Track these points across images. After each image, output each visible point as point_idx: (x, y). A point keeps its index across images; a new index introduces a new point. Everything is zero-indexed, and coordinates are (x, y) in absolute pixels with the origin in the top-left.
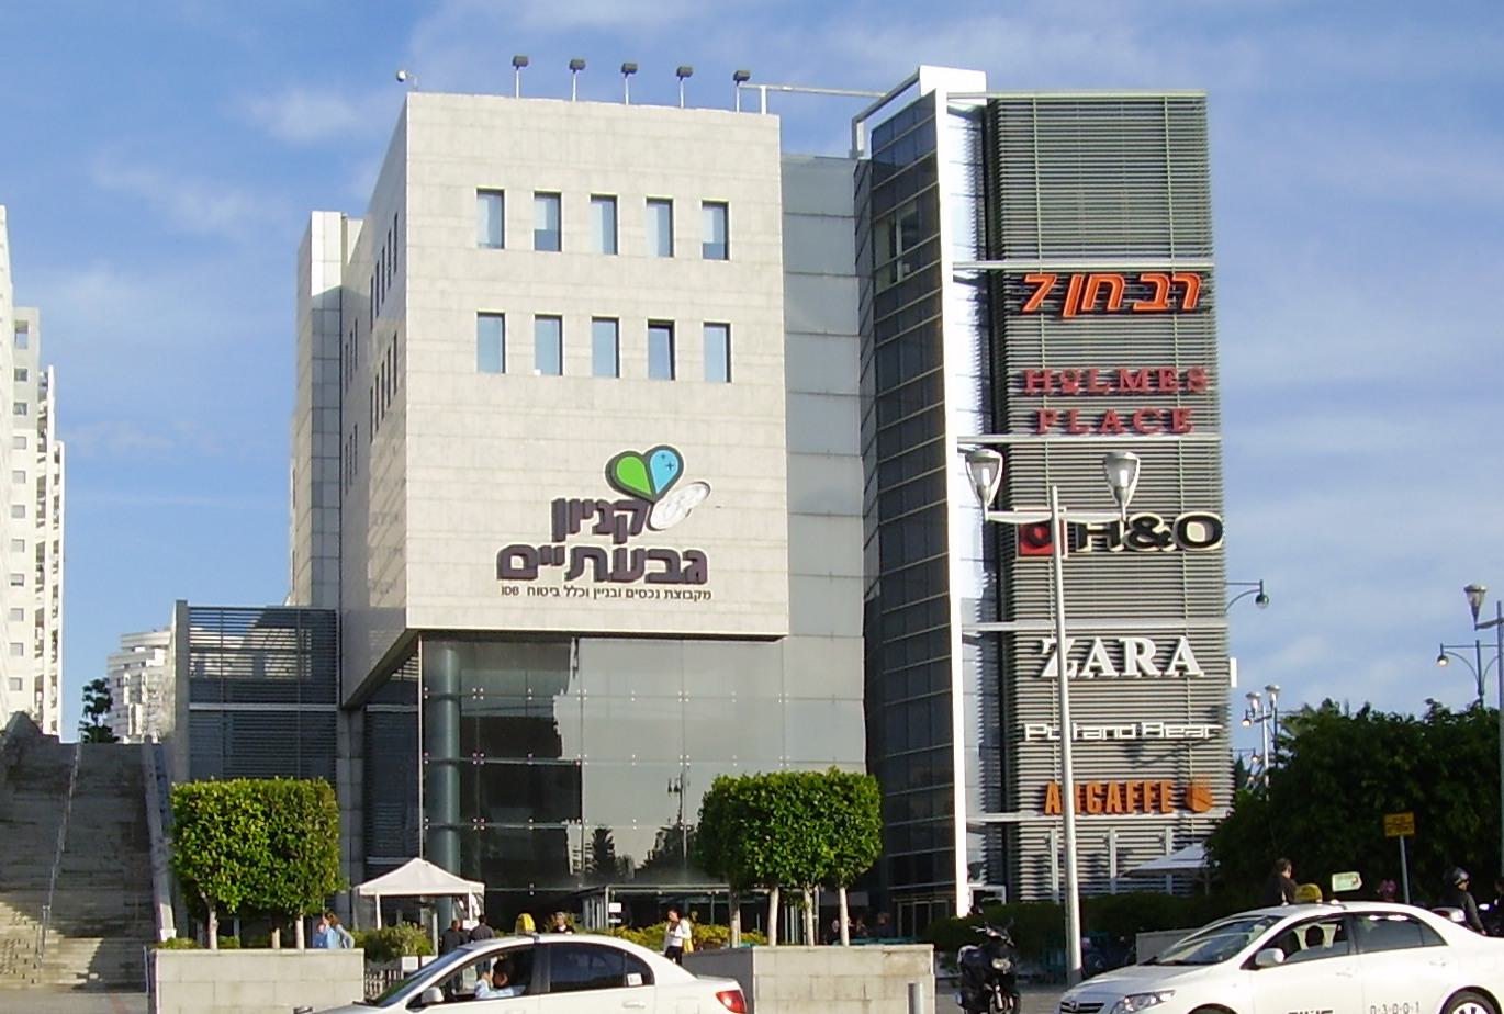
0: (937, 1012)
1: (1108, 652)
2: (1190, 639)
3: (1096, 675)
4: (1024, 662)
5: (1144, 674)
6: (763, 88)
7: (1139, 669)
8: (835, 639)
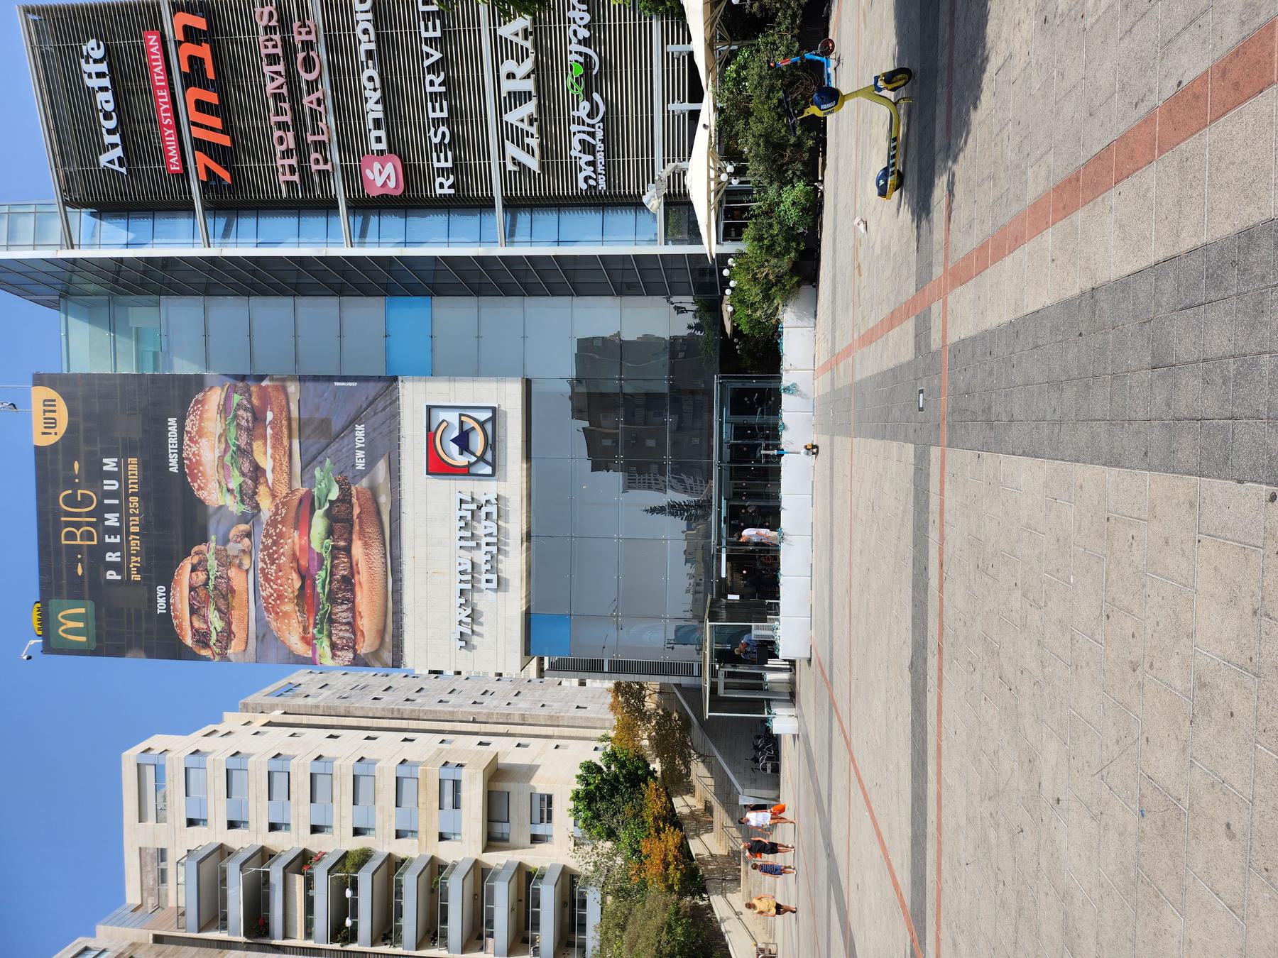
0: (985, 4)
1: (516, 107)
2: (500, 25)
3: (536, 120)
4: (526, 188)
5: (533, 72)
6: (763, 452)
7: (528, 76)
8: (527, 335)
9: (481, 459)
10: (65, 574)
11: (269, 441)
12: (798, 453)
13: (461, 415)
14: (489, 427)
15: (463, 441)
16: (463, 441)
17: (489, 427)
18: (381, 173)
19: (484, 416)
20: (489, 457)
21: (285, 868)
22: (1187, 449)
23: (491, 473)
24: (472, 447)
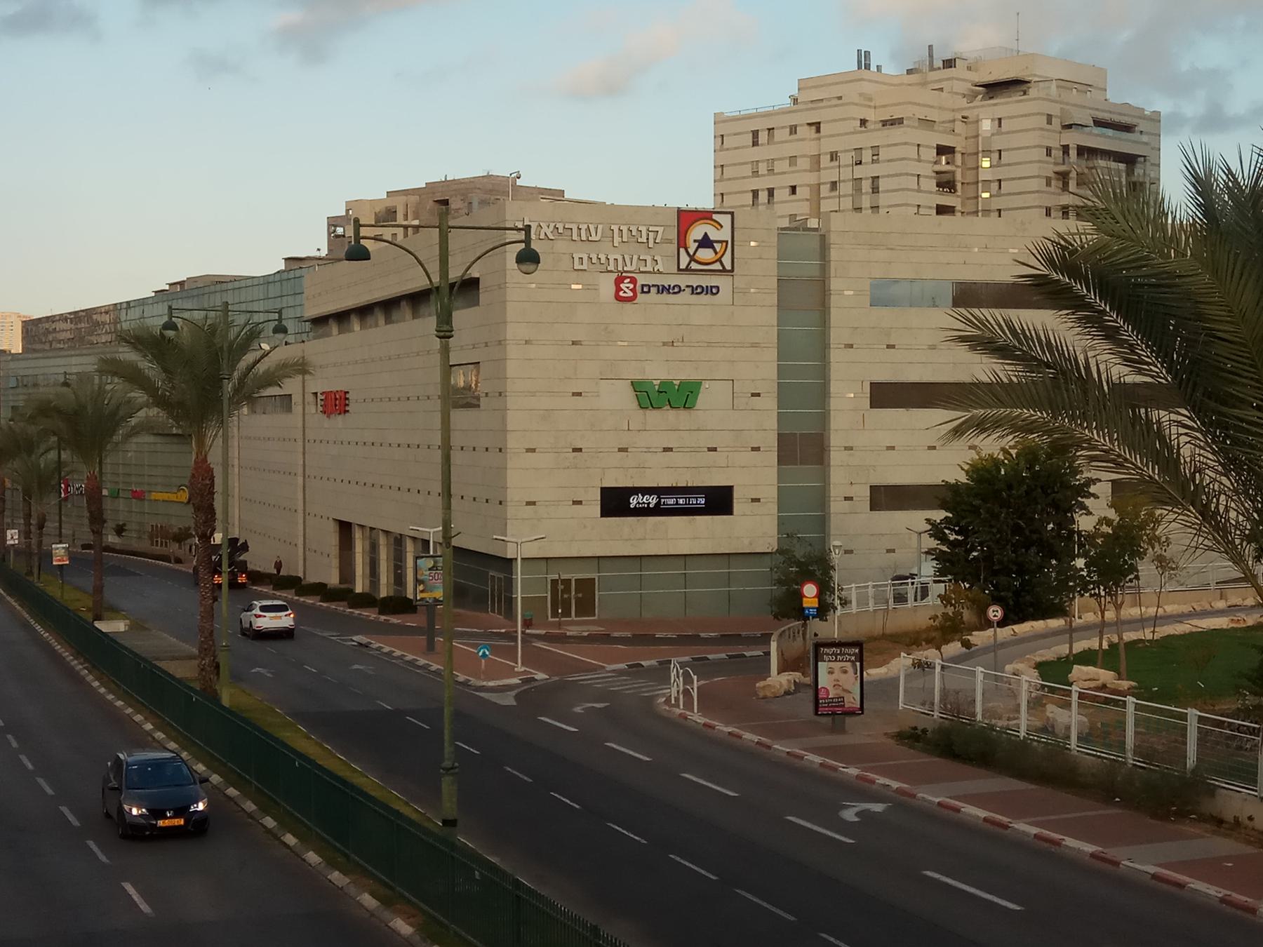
11: (237, 523)
12: (882, 296)
13: (727, 242)
14: (717, 266)
15: (706, 242)
16: (706, 242)
18: (628, 288)
19: (727, 260)
20: (694, 266)
21: (827, 690)
22: (119, 306)
23: (681, 267)
24: (700, 250)
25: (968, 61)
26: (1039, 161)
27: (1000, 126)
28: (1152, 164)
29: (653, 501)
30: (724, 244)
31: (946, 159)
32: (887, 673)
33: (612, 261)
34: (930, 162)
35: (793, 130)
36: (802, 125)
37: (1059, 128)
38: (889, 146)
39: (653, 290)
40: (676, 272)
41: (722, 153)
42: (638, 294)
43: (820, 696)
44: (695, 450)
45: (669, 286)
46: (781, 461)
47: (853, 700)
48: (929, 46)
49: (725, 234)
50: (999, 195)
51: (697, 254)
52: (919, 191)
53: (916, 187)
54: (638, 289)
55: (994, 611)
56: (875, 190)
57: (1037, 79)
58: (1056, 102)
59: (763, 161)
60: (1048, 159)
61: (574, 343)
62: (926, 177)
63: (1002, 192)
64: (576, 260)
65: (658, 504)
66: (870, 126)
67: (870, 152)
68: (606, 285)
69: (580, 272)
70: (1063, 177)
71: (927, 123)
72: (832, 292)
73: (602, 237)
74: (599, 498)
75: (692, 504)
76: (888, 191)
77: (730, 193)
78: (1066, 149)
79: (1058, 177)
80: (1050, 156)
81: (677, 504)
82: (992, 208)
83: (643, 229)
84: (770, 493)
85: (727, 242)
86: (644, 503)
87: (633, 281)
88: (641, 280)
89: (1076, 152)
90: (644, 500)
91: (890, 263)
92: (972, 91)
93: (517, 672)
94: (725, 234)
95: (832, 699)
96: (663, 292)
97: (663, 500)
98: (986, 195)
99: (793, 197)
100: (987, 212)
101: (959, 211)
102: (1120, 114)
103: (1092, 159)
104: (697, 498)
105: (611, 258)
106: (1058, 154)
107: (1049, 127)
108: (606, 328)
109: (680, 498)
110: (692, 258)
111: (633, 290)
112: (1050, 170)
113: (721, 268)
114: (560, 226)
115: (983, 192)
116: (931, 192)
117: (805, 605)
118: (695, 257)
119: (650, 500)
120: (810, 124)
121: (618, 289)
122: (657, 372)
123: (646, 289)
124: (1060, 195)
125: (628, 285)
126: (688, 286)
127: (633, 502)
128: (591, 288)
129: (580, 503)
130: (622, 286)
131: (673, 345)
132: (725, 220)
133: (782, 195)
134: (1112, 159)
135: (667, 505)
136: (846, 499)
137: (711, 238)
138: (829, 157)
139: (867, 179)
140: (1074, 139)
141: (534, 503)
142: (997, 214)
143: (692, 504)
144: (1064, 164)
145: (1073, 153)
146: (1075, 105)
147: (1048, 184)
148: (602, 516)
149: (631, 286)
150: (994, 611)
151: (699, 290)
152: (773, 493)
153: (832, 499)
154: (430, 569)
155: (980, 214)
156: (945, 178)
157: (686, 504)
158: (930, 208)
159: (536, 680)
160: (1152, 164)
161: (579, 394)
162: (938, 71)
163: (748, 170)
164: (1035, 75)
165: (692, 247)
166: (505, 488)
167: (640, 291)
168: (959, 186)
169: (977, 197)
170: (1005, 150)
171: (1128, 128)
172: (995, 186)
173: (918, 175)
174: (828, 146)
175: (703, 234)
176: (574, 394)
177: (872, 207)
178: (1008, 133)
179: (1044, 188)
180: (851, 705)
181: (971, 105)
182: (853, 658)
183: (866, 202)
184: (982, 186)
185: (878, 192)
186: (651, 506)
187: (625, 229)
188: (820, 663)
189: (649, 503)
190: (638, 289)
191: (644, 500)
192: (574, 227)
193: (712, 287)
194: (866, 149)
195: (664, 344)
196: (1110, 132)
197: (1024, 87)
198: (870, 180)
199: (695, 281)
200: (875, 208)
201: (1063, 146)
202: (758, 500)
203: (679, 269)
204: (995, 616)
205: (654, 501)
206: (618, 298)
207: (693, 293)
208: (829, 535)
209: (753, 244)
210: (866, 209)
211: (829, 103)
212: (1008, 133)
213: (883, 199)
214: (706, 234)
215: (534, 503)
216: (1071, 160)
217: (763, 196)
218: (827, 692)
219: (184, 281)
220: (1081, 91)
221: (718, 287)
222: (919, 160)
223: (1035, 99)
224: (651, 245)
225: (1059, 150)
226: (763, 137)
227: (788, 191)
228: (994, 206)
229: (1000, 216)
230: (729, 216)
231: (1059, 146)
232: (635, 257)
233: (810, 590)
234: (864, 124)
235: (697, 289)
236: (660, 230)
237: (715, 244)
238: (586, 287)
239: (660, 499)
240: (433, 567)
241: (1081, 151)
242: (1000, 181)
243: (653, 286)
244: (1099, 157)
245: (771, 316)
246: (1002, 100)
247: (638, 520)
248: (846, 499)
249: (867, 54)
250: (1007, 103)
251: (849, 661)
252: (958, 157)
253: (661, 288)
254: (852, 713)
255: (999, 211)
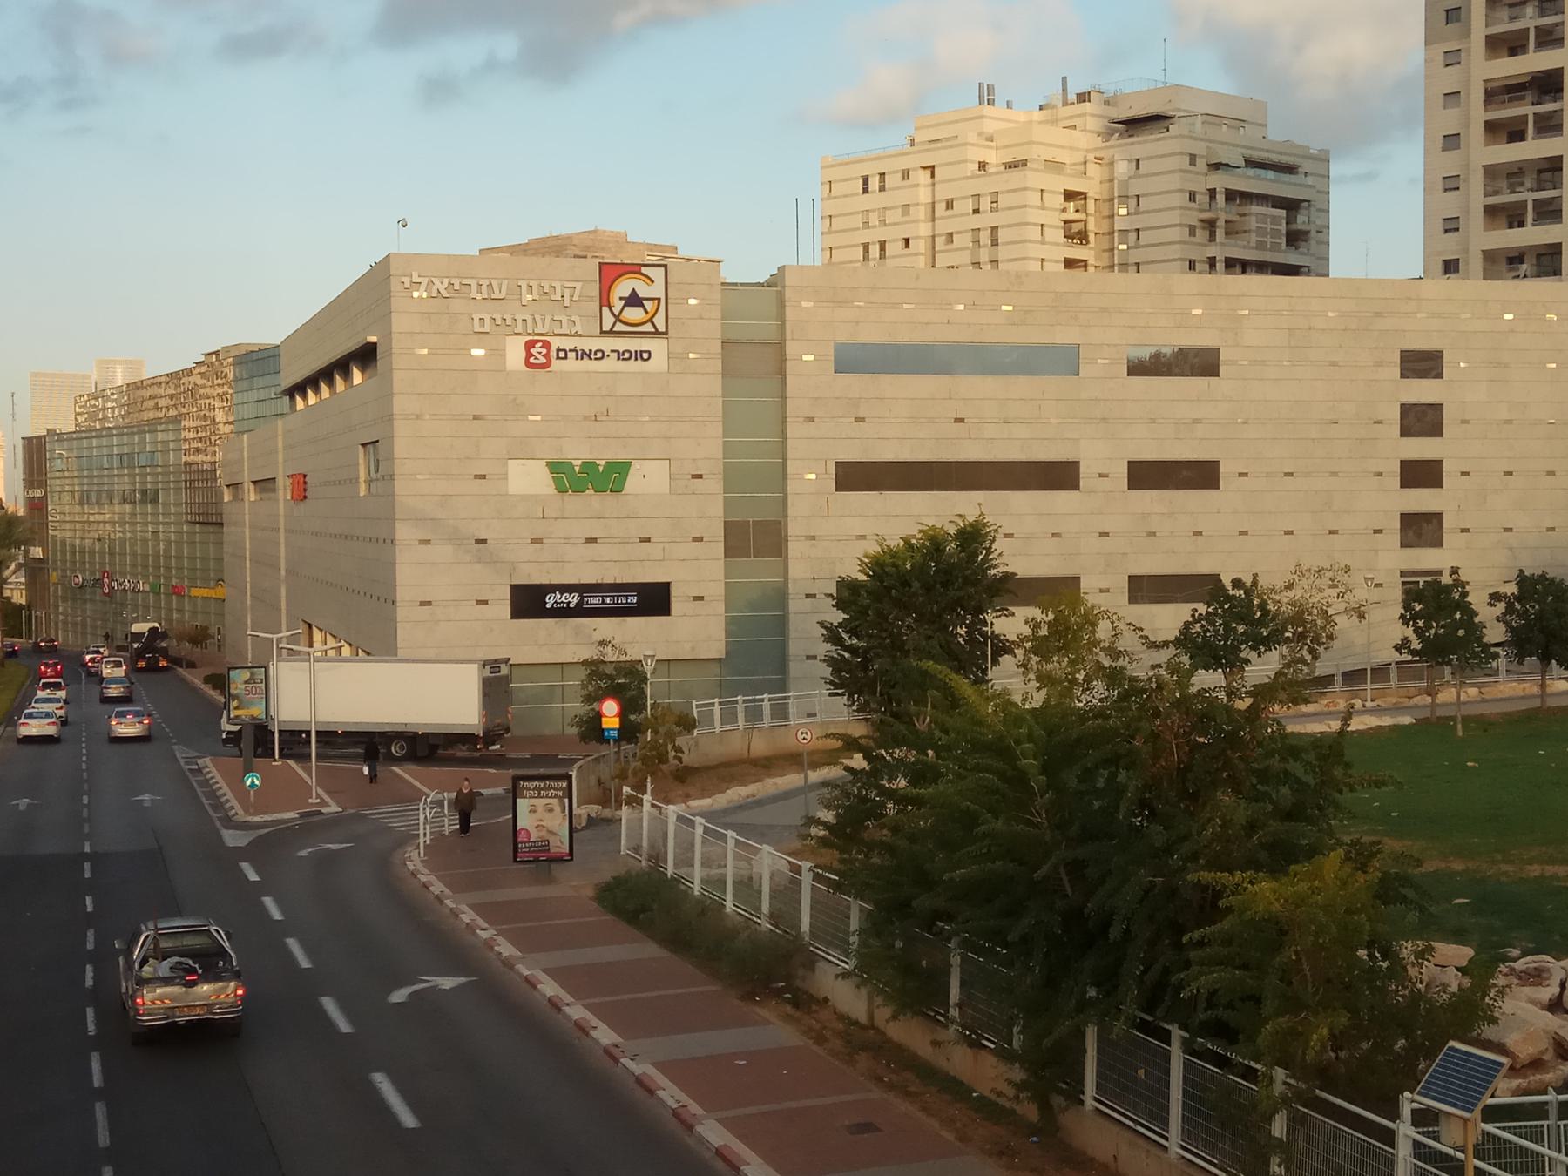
9: (618, 319)
10: (352, 750)
12: (851, 360)
13: (659, 299)
14: (648, 328)
15: (634, 300)
17: (648, 328)
18: (540, 353)
19: (660, 321)
20: (619, 327)
23: (604, 329)
25: (1105, 95)
26: (1181, 208)
27: (1138, 167)
28: (1319, 210)
29: (573, 599)
30: (656, 301)
31: (1075, 206)
32: (712, 805)
33: (519, 323)
34: (1056, 210)
35: (906, 174)
36: (914, 169)
37: (1205, 169)
38: (1008, 191)
39: (572, 355)
40: (599, 334)
41: (828, 202)
42: (554, 360)
43: (519, 840)
44: (625, 541)
45: (590, 351)
46: (729, 552)
47: (560, 844)
48: (1063, 78)
49: (657, 290)
50: (1137, 247)
51: (623, 314)
52: (1043, 242)
53: (1040, 238)
54: (553, 354)
55: (802, 733)
56: (995, 242)
57: (1182, 114)
58: (1202, 140)
59: (874, 211)
60: (1192, 205)
61: (476, 417)
62: (1051, 226)
63: (1142, 243)
64: (476, 321)
65: (580, 603)
66: (991, 169)
67: (989, 199)
68: (515, 352)
69: (481, 335)
70: (1211, 225)
71: (1054, 166)
72: (788, 357)
73: (507, 294)
74: (509, 597)
75: (622, 603)
76: (1008, 243)
77: (1148, 263)
78: (1212, 193)
79: (1203, 224)
80: (1194, 201)
81: (603, 603)
82: (1130, 262)
83: (558, 285)
84: (715, 589)
85: (659, 299)
86: (562, 602)
87: (547, 345)
88: (556, 343)
89: (1224, 196)
90: (563, 599)
91: (857, 323)
92: (1109, 128)
93: (312, 804)
94: (657, 290)
95: (535, 842)
96: (582, 359)
97: (585, 599)
98: (1124, 247)
99: (907, 251)
100: (1124, 266)
101: (1092, 265)
102: (1281, 153)
103: (1246, 205)
104: (627, 596)
105: (519, 318)
106: (1203, 199)
107: (1192, 168)
108: (515, 399)
109: (607, 596)
110: (618, 319)
111: (547, 356)
112: (1194, 218)
113: (653, 330)
114: (457, 282)
115: (1120, 244)
116: (1057, 244)
117: (604, 726)
118: (621, 318)
119: (570, 599)
120: (924, 168)
121: (529, 355)
122: (577, 453)
123: (562, 354)
124: (1205, 245)
125: (540, 350)
126: (612, 351)
127: (550, 601)
128: (497, 354)
129: (485, 602)
130: (532, 350)
131: (596, 420)
132: (657, 274)
133: (894, 248)
134: (1270, 205)
135: (591, 604)
136: (808, 596)
137: (640, 296)
138: (944, 204)
139: (985, 229)
140: (1221, 181)
141: (429, 603)
142: (1135, 268)
143: (622, 603)
144: (1210, 210)
145: (1220, 198)
146: (1223, 143)
147: (1192, 232)
148: (512, 618)
149: (544, 351)
150: (802, 733)
151: (627, 355)
152: (719, 590)
153: (791, 597)
154: (246, 682)
155: (1116, 268)
156: (1076, 228)
157: (614, 603)
158: (1057, 261)
159: (323, 814)
160: (1319, 210)
161: (483, 477)
162: (1073, 106)
163: (857, 221)
164: (1179, 110)
165: (618, 305)
166: (394, 587)
167: (555, 357)
168: (1092, 237)
169: (1112, 250)
170: (1144, 195)
171: (1290, 169)
172: (1133, 236)
173: (1042, 225)
174: (943, 193)
175: (631, 290)
176: (477, 477)
177: (991, 262)
178: (1147, 175)
179: (1186, 237)
180: (557, 850)
181: (1107, 144)
182: (560, 793)
183: (984, 255)
184: (1119, 236)
185: (997, 245)
186: (571, 606)
187: (534, 284)
188: (518, 800)
189: (569, 602)
190: (553, 354)
191: (563, 599)
192: (473, 283)
193: (641, 352)
194: (984, 195)
195: (586, 418)
196: (1271, 174)
197: (1166, 123)
198: (989, 231)
199: (622, 344)
200: (995, 262)
201: (1209, 190)
202: (701, 598)
203: (602, 332)
204: (804, 739)
205: (575, 600)
206: (528, 364)
207: (619, 359)
208: (788, 638)
209: (692, 302)
210: (985, 263)
211: (949, 143)
212: (1147, 175)
213: (1003, 252)
214: (634, 289)
215: (429, 603)
216: (1219, 206)
217: (875, 251)
218: (529, 835)
219: (218, 351)
220: (1233, 127)
221: (649, 352)
222: (1043, 208)
223: (1176, 137)
224: (567, 302)
225: (1205, 194)
226: (874, 183)
227: (901, 244)
228: (1132, 260)
229: (1138, 272)
230: (663, 269)
231: (1204, 190)
232: (548, 319)
233: (610, 708)
234: (984, 166)
235: (623, 354)
236: (578, 285)
237: (644, 302)
238: (434, 351)
239: (582, 598)
240: (249, 679)
241: (1231, 196)
242: (1138, 230)
243: (570, 350)
244: (1254, 202)
245: (716, 385)
246: (1140, 139)
247: (556, 623)
248: (808, 596)
249: (991, 89)
250: (1145, 142)
251: (556, 796)
252: (1091, 205)
253: (580, 353)
254: (559, 859)
255: (1138, 265)
